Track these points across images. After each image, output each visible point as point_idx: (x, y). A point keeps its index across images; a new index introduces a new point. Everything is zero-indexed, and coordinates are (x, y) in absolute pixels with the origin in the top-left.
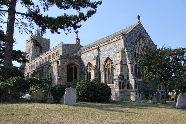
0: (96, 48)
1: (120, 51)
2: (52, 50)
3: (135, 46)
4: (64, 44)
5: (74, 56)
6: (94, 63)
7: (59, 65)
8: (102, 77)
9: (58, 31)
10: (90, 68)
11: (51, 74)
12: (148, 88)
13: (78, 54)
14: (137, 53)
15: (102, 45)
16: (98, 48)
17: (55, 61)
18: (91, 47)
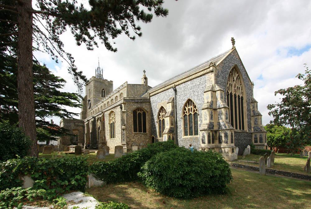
0: (172, 87)
1: (171, 101)
2: (115, 92)
3: (228, 82)
4: (129, 84)
5: (141, 99)
6: (169, 108)
7: (123, 110)
10: (163, 114)
11: (113, 122)
12: (242, 140)
13: (146, 95)
14: (230, 92)
15: (180, 82)
16: (175, 88)
17: (117, 106)
18: (164, 88)
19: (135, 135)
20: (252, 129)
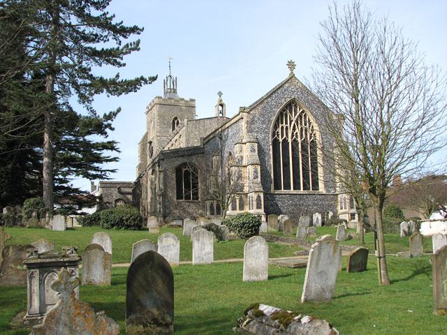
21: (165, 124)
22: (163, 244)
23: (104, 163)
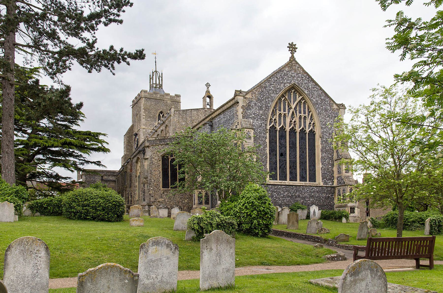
8: (318, 146)
9: (394, 39)
19: (163, 193)
20: (335, 181)
21: (150, 117)
22: (150, 258)
23: (94, 153)
